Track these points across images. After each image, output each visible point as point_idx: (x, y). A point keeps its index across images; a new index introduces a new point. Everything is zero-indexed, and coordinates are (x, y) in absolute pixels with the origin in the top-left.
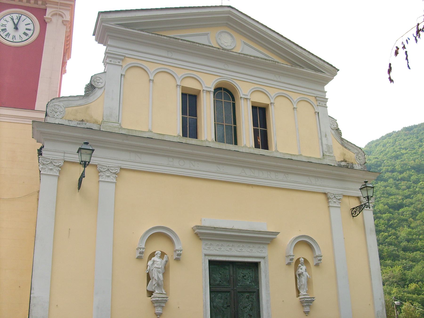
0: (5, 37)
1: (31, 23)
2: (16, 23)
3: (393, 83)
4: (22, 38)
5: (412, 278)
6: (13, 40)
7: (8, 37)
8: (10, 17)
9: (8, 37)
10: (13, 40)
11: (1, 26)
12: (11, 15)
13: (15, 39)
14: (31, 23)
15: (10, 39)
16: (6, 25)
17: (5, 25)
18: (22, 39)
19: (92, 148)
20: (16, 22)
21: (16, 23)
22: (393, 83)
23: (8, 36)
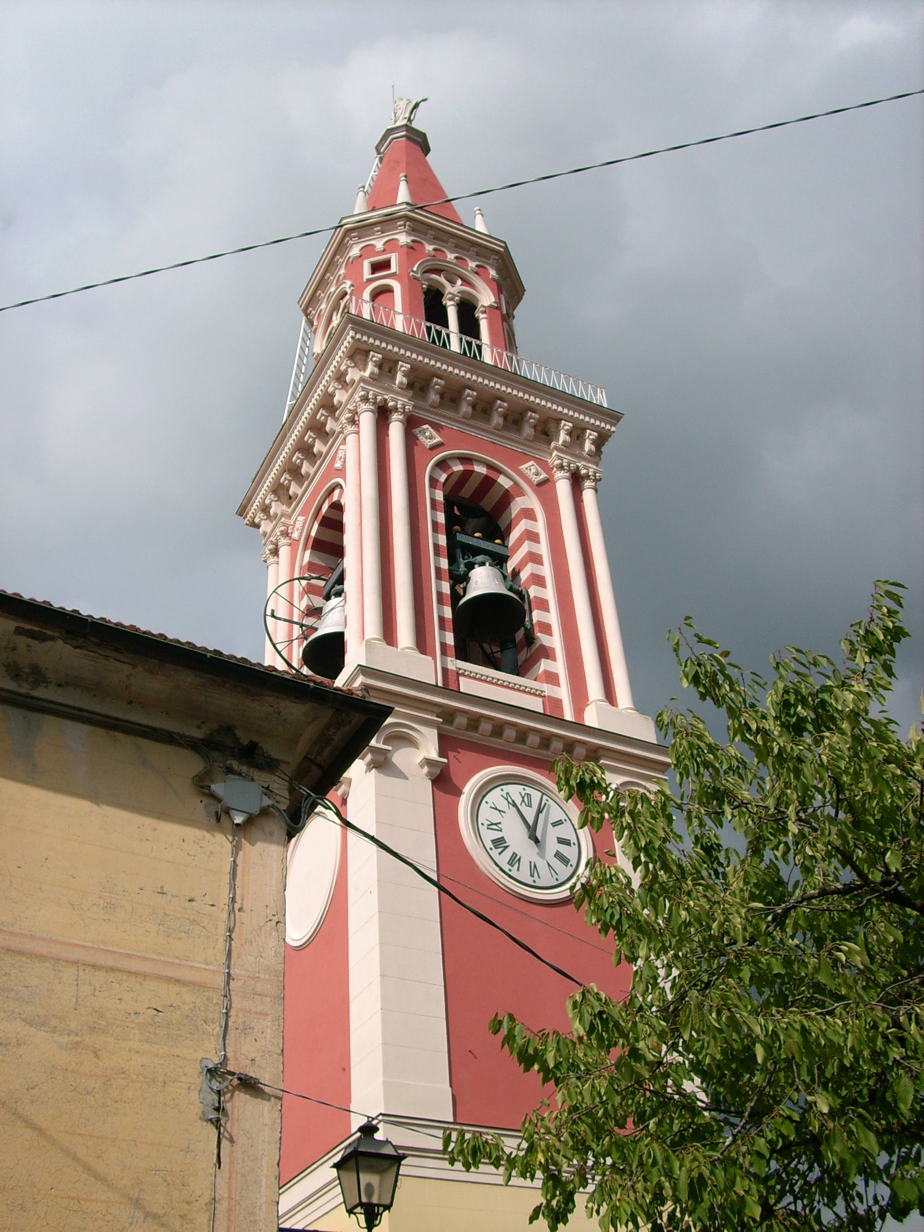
0: (491, 849)
1: (574, 844)
2: (531, 823)
3: (531, 1222)
4: (557, 874)
5: (352, 333)
6: (510, 867)
7: (500, 853)
8: (520, 793)
9: (500, 853)
10: (510, 870)
11: (488, 828)
12: (524, 789)
13: (518, 869)
14: (574, 844)
15: (503, 860)
16: (500, 823)
17: (507, 799)
18: (557, 877)
19: (438, 879)
20: (530, 816)
21: (531, 823)
22: (531, 1222)
23: (500, 850)
